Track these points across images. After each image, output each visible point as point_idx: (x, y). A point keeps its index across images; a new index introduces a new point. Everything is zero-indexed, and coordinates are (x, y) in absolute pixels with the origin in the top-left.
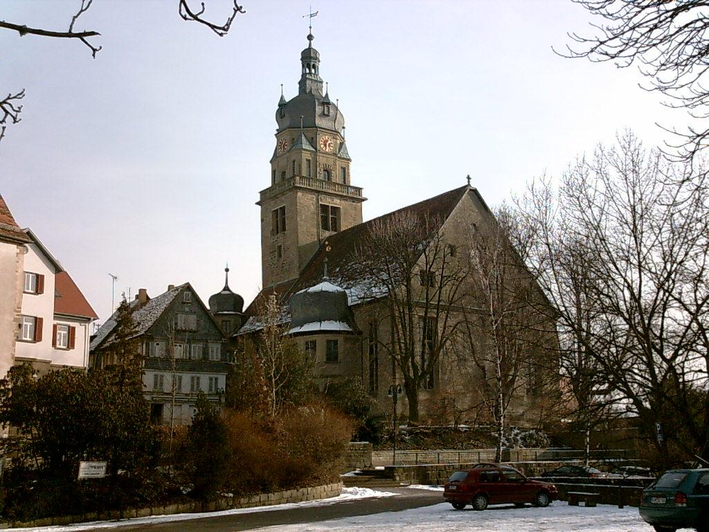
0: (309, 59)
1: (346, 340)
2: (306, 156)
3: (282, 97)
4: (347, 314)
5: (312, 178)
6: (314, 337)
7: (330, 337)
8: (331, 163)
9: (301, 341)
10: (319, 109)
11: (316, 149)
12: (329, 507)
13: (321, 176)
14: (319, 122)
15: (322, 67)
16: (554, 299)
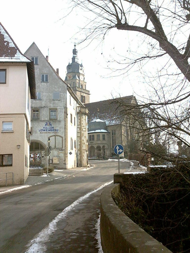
0: (75, 52)
1: (107, 134)
2: (77, 81)
3: (69, 63)
4: (106, 128)
5: (79, 88)
6: (94, 134)
7: (104, 134)
8: (83, 84)
9: (95, 134)
10: (80, 68)
11: (79, 79)
12: (42, 229)
13: (81, 87)
14: (80, 71)
15: (78, 54)
16: (97, 144)
